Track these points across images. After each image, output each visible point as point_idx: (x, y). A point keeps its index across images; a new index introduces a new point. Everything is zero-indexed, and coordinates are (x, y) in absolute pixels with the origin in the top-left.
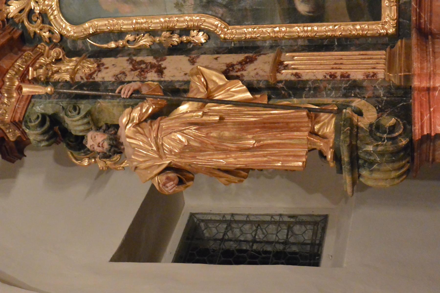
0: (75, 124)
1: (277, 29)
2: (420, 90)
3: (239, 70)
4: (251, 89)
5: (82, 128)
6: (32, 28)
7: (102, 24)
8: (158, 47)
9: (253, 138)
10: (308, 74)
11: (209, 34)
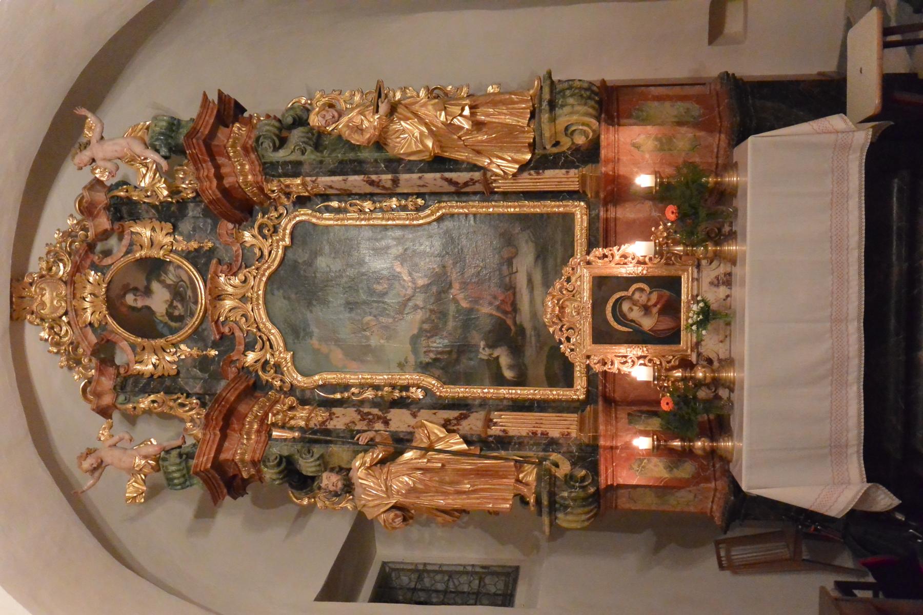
0: (307, 466)
1: (486, 390)
2: (605, 448)
3: (455, 425)
4: (467, 441)
5: (313, 469)
6: (264, 377)
7: (331, 377)
8: (379, 400)
9: (468, 483)
10: (513, 431)
11: (426, 390)
